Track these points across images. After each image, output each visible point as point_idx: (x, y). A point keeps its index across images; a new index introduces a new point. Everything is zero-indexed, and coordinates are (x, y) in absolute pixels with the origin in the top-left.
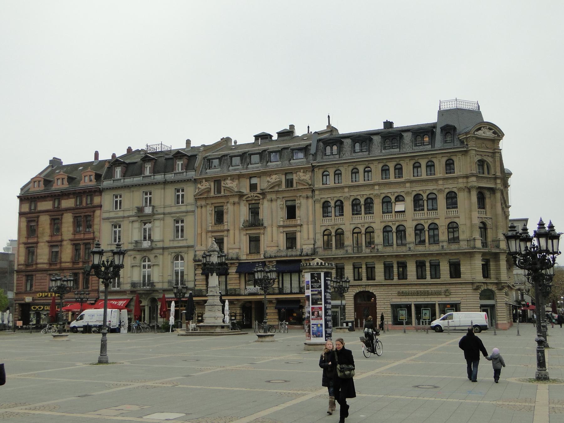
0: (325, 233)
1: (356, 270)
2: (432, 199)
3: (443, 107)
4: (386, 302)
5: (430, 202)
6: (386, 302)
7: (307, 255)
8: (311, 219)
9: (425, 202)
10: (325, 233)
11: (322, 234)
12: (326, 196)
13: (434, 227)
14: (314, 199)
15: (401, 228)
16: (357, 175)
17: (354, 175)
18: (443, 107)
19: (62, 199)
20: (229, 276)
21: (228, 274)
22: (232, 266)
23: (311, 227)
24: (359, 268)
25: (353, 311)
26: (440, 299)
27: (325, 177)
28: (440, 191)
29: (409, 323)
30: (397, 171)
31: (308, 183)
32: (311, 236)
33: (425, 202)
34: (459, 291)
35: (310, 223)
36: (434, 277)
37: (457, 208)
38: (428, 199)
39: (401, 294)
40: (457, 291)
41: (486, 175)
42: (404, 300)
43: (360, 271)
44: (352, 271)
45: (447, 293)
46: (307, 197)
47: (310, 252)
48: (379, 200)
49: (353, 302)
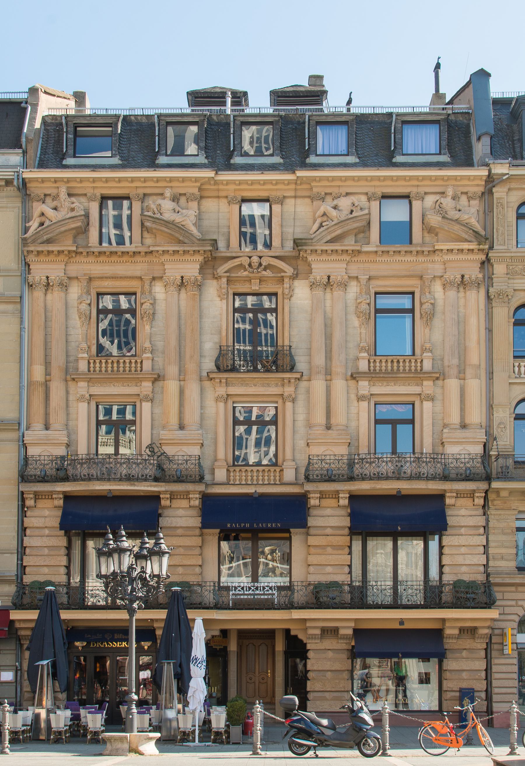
22: (326, 502)
35: (469, 372)
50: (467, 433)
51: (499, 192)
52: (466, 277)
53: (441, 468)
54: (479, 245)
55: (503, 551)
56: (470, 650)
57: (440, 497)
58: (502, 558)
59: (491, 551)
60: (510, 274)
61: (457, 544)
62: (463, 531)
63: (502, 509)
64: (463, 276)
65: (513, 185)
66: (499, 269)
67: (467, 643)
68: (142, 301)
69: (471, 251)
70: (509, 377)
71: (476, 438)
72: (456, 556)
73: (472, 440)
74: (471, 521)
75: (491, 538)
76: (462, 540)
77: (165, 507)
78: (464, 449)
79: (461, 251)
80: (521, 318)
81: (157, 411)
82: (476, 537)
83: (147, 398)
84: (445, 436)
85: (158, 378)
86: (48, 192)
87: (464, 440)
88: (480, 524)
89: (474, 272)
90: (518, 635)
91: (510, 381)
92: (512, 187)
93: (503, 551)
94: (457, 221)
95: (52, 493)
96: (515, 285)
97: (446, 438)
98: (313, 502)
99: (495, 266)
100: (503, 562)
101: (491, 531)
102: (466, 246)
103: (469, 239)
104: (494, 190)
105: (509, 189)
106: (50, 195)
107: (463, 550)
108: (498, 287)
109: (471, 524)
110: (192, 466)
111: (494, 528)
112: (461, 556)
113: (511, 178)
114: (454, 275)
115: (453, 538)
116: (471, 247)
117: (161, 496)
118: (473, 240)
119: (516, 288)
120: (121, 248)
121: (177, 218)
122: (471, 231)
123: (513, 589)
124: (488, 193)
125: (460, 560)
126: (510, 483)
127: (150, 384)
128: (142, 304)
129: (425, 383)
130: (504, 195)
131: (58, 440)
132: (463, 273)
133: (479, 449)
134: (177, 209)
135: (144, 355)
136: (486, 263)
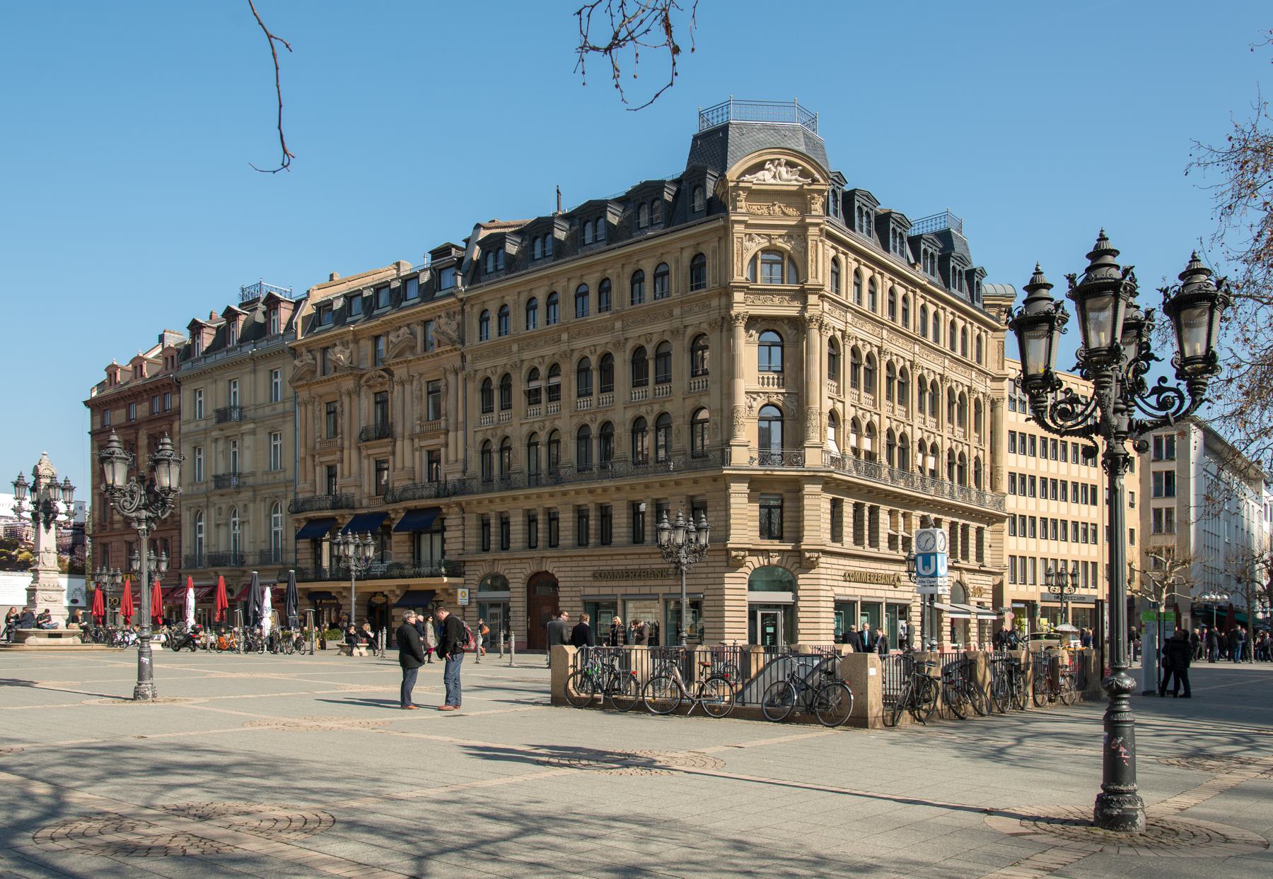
23: (460, 433)
27: (580, 300)
31: (450, 339)
32: (461, 456)
37: (670, 381)
39: (599, 576)
51: (467, 308)
66: (469, 358)
85: (447, 432)
89: (458, 364)
98: (444, 511)
136: (463, 357)
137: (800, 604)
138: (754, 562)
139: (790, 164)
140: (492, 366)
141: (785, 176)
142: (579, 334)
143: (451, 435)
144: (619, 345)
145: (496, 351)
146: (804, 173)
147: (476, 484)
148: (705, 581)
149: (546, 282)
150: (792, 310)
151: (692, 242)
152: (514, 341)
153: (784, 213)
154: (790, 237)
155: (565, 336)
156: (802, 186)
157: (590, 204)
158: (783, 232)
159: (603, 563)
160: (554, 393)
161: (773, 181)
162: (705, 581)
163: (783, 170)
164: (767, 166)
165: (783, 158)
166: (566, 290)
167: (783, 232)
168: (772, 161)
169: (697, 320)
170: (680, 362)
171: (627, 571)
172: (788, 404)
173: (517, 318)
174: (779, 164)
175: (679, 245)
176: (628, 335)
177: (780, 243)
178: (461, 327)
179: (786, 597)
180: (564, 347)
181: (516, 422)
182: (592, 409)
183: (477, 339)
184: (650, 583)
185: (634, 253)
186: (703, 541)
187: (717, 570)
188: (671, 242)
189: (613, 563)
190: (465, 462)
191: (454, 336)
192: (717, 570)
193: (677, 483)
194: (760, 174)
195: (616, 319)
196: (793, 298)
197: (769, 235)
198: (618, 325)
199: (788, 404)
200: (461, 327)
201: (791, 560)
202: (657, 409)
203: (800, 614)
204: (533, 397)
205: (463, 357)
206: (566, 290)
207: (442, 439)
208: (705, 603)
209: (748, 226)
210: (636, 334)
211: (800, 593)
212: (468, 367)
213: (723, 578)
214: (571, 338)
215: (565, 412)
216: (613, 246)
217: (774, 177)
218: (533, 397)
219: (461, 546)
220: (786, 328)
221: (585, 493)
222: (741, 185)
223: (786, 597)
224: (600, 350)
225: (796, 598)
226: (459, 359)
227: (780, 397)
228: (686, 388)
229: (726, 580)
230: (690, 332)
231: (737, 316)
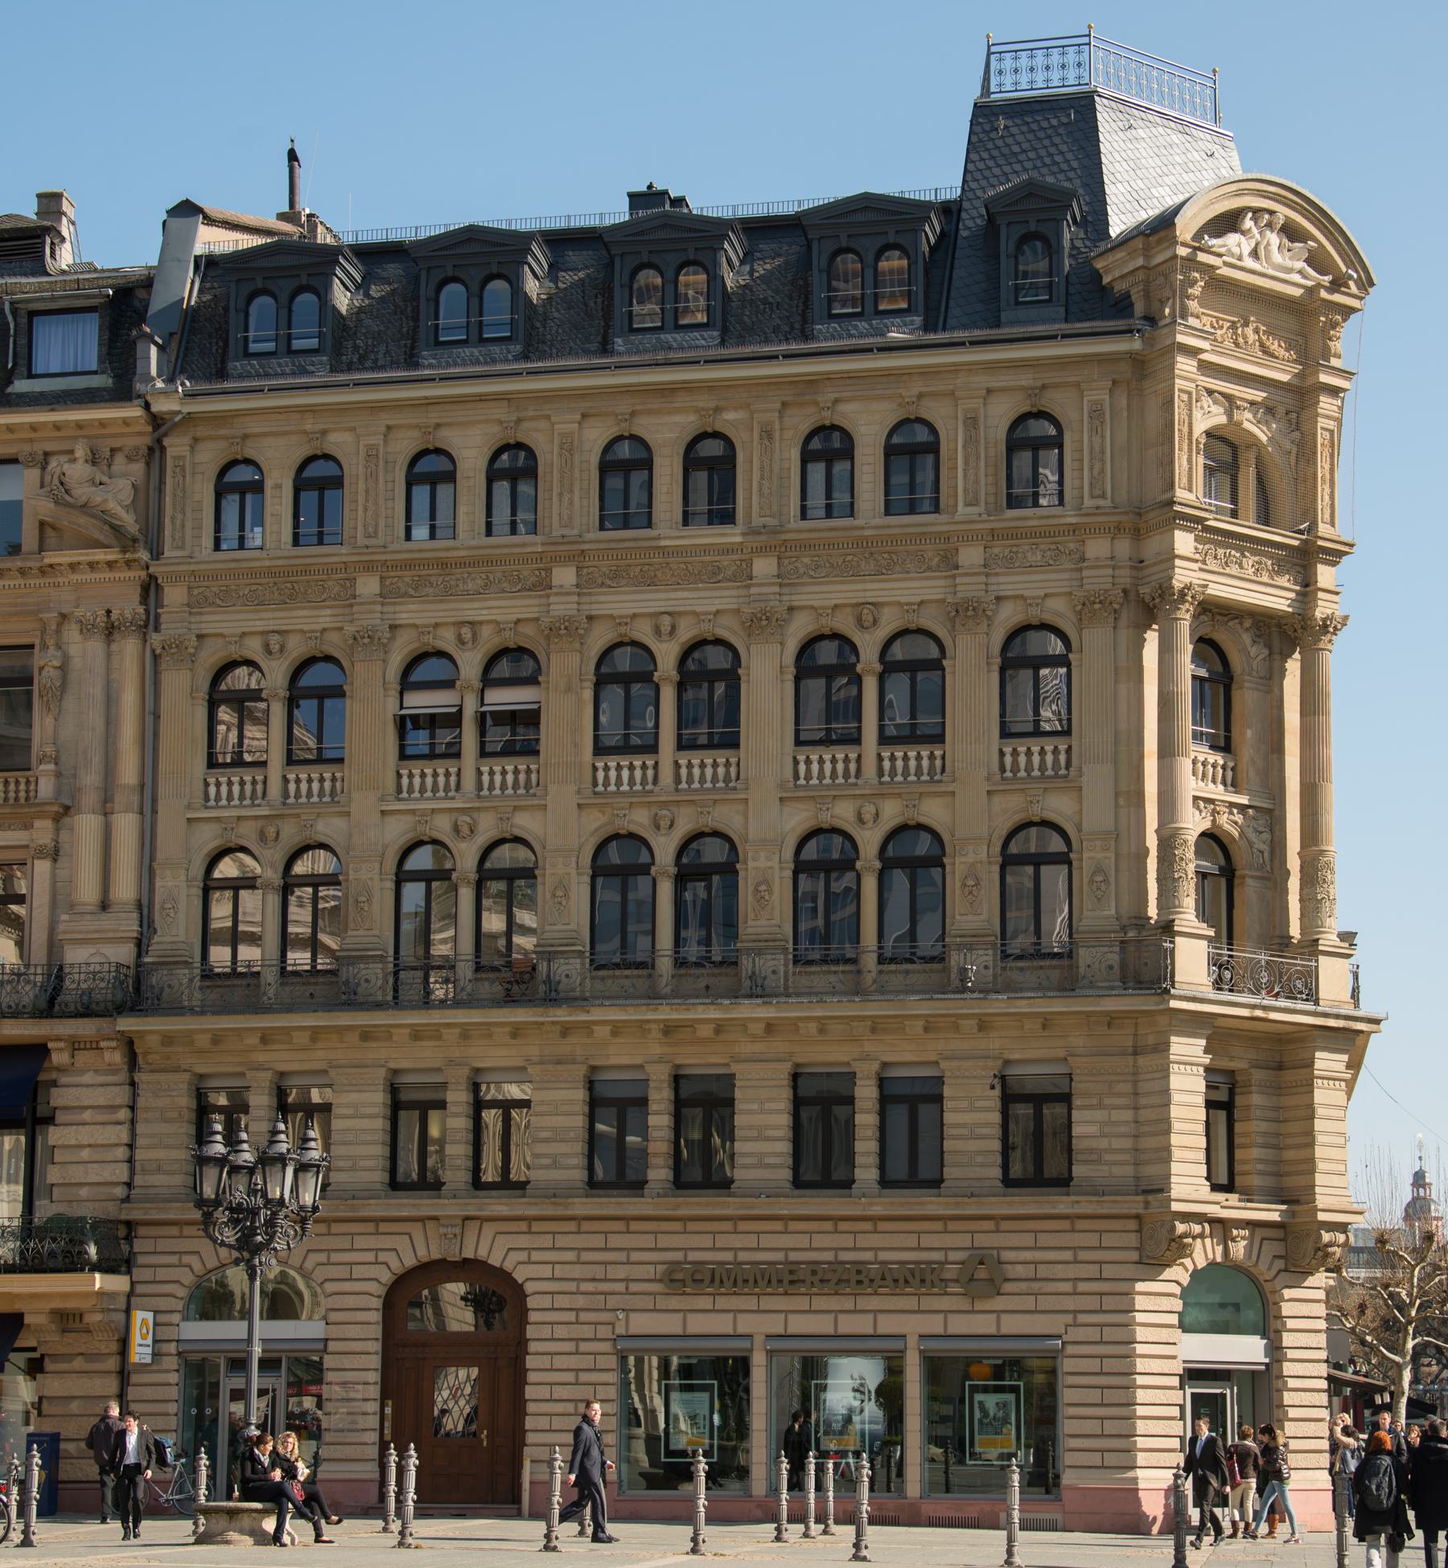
0: (412, 864)
1: (409, 1120)
2: (912, 667)
3: (1008, 81)
4: (587, 1330)
5: (900, 683)
6: (587, 1330)
7: (87, 1011)
8: (128, 772)
9: (870, 687)
10: (412, 864)
11: (391, 866)
12: (234, 626)
13: (709, 868)
14: (155, 639)
15: (713, 852)
16: (443, 490)
17: (421, 493)
18: (1008, 81)
19: (101, 317)
20: (55, 1135)
21: (50, 1120)
22: (83, 1058)
23: (126, 825)
24: (424, 1108)
25: (374, 1392)
26: (934, 1324)
27: (231, 503)
28: (964, 612)
29: (728, 1469)
30: (701, 478)
31: (117, 530)
32: (125, 888)
33: (870, 687)
34: (1060, 1271)
35: (120, 799)
36: (697, 1174)
37: (735, 745)
38: (889, 668)
39: (686, 1279)
40: (1043, 1271)
41: (1247, 527)
42: (711, 1321)
43: (434, 1131)
44: (380, 1124)
45: (983, 1277)
46: (110, 631)
47: (103, 992)
48: (574, 659)
49: (377, 1331)
50: (106, 922)
51: (176, 446)
52: (114, 615)
53: (31, 994)
54: (125, 552)
55: (161, 1154)
56: (88, 1357)
57: (39, 1051)
58: (159, 1170)
59: (139, 1155)
60: (195, 605)
61: (73, 1142)
62: (87, 1115)
63: (164, 1071)
64: (109, 612)
65: (201, 431)
66: (174, 596)
67: (76, 1343)
68: (42, 663)
69: (110, 565)
70: (189, 807)
71: (117, 931)
72: (69, 1167)
73: (110, 935)
74: (100, 1097)
75: (140, 1128)
76: (84, 1135)
77: (60, 1070)
78: (97, 954)
79: (92, 566)
80: (312, 684)
81: (62, 874)
82: (109, 1128)
83: (40, 853)
84: (61, 927)
85: (64, 812)
86: (117, 444)
87: (97, 936)
88: (118, 1101)
89: (129, 606)
90: (182, 1324)
91: (384, 808)
92: (198, 434)
93: (161, 1154)
94: (84, 507)
95: (287, 1031)
96: (594, 606)
97: (65, 932)
98: (59, 1058)
99: (166, 590)
100: (160, 1177)
101: (141, 1115)
102: (100, 555)
103: (106, 542)
104: (166, 442)
105: (196, 440)
106: (120, 449)
107: (85, 1154)
108: (172, 632)
109: (102, 1101)
110: (103, 985)
111: (147, 1109)
112: (81, 1167)
113: (189, 418)
114: (91, 610)
115: (67, 1130)
116: (111, 557)
117: (50, 1045)
118: (114, 542)
119: (1001, 594)
120: (372, 542)
121: (97, 496)
122: (107, 527)
123: (174, 1230)
124: (155, 452)
125: (77, 1174)
126: (290, 1016)
127: (48, 824)
128: (41, 669)
129: (37, 824)
130: (185, 451)
131: (117, 931)
132: (108, 606)
133: (124, 953)
134: (99, 477)
135: (42, 767)
136: (150, 589)
137: (1288, 1368)
138: (1204, 1252)
139: (1291, 232)
140: (270, 633)
141: (1277, 257)
142: (616, 575)
143: (87, 825)
144: (762, 623)
145: (286, 587)
146: (1317, 261)
147: (374, 977)
148: (1069, 1303)
149: (500, 411)
150: (1277, 597)
151: (1026, 379)
152: (369, 567)
153: (1265, 351)
154: (1268, 410)
155: (565, 576)
156: (1311, 291)
157: (472, 236)
158: (1259, 395)
159: (847, 1241)
160: (518, 733)
161: (1249, 263)
162: (1069, 1303)
163: (1274, 239)
164: (1248, 223)
165: (1283, 212)
166: (570, 446)
167: (1259, 395)
168: (1256, 211)
169: (1038, 588)
170: (971, 689)
171: (792, 1267)
172: (1252, 836)
173: (373, 504)
174: (1269, 225)
175: (984, 380)
176: (799, 600)
177: (1248, 421)
178: (150, 500)
179: (1246, 1350)
180: (562, 607)
181: (363, 804)
182: (665, 797)
183: (208, 541)
184: (874, 1303)
185: (828, 377)
186: (308, 1198)
187: (1109, 1271)
188: (971, 368)
189: (737, 1241)
190: (145, 909)
191: (129, 521)
192: (1109, 1271)
193: (983, 1024)
194: (1232, 239)
195: (763, 550)
196: (1280, 568)
197: (1229, 398)
198: (764, 567)
199: (1252, 836)
200: (150, 500)
201: (1270, 1249)
202: (892, 813)
203: (1288, 1398)
204: (424, 737)
205: (150, 589)
206: (568, 447)
207: (42, 832)
208: (1067, 1365)
209: (1206, 368)
210: (825, 600)
211: (1287, 1339)
212: (173, 625)
213: (1129, 1294)
214: (584, 585)
215: (562, 794)
216: (342, 377)
217: (1254, 253)
218: (424, 737)
219: (121, 1173)
220: (1247, 638)
221: (641, 1039)
222: (1202, 257)
223: (1246, 1350)
224: (687, 632)
225: (1275, 1350)
226: (135, 594)
227: (1239, 818)
228: (789, 773)
229: (1140, 1302)
230: (1009, 616)
231: (1182, 595)
